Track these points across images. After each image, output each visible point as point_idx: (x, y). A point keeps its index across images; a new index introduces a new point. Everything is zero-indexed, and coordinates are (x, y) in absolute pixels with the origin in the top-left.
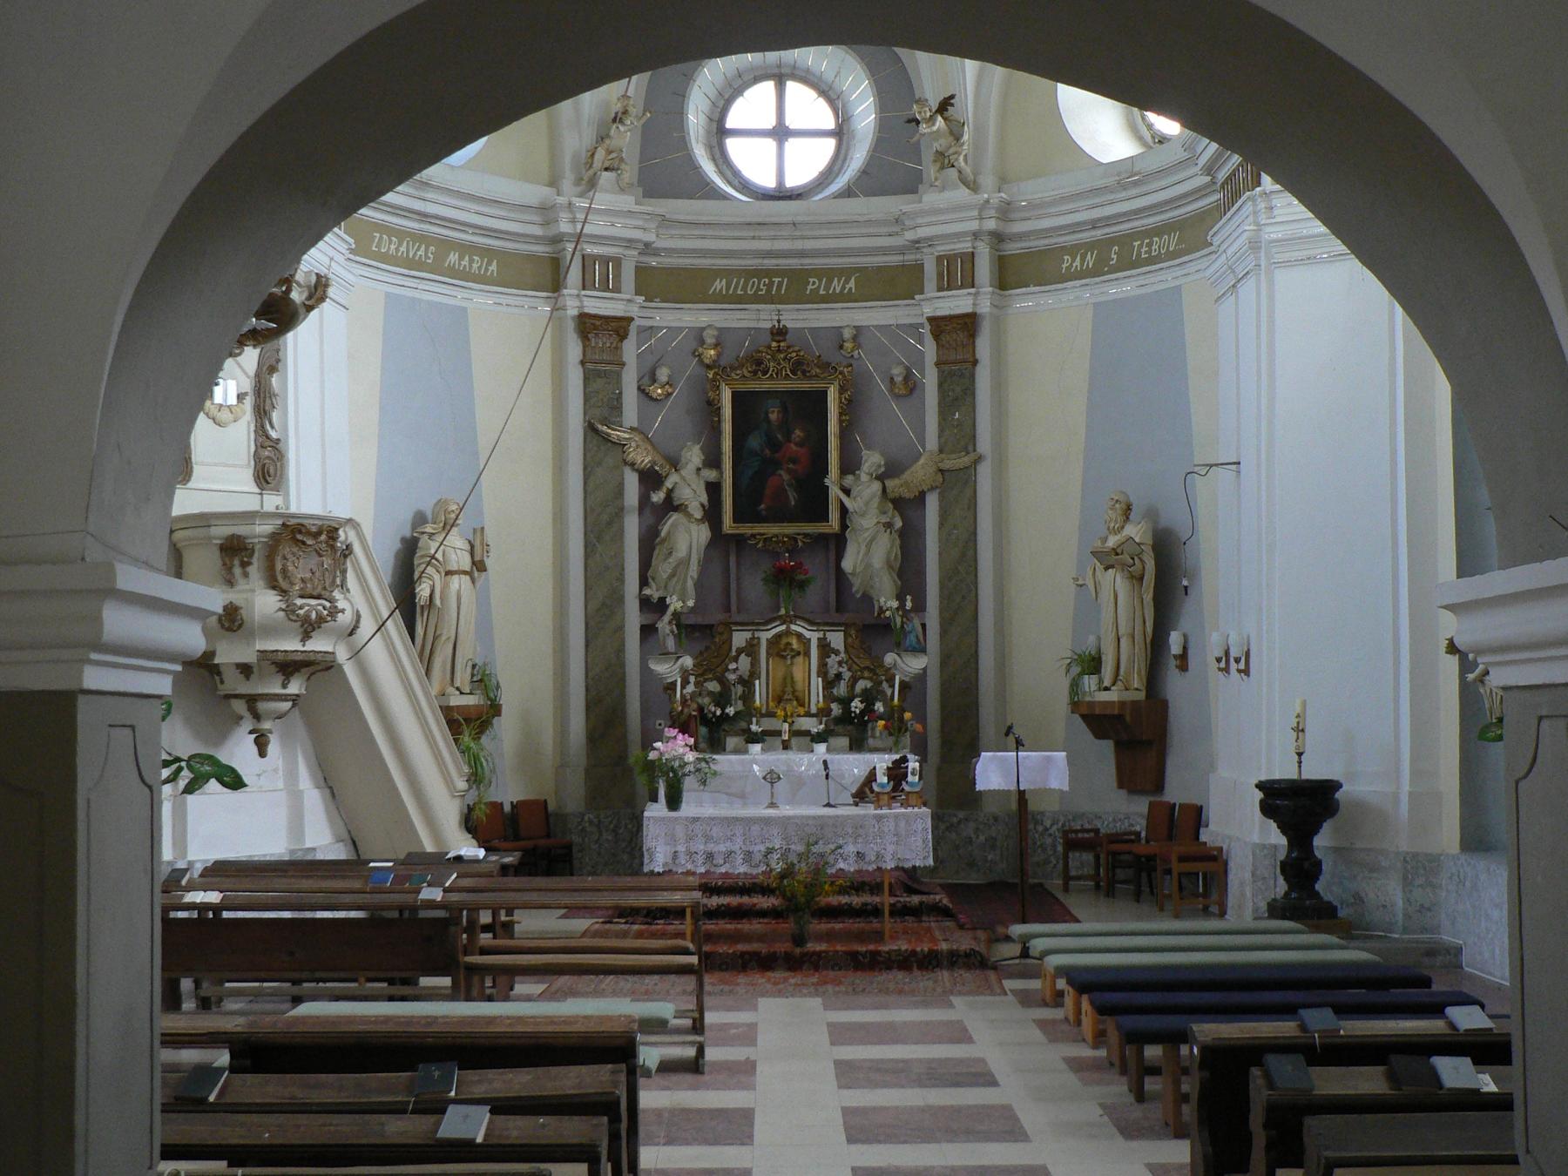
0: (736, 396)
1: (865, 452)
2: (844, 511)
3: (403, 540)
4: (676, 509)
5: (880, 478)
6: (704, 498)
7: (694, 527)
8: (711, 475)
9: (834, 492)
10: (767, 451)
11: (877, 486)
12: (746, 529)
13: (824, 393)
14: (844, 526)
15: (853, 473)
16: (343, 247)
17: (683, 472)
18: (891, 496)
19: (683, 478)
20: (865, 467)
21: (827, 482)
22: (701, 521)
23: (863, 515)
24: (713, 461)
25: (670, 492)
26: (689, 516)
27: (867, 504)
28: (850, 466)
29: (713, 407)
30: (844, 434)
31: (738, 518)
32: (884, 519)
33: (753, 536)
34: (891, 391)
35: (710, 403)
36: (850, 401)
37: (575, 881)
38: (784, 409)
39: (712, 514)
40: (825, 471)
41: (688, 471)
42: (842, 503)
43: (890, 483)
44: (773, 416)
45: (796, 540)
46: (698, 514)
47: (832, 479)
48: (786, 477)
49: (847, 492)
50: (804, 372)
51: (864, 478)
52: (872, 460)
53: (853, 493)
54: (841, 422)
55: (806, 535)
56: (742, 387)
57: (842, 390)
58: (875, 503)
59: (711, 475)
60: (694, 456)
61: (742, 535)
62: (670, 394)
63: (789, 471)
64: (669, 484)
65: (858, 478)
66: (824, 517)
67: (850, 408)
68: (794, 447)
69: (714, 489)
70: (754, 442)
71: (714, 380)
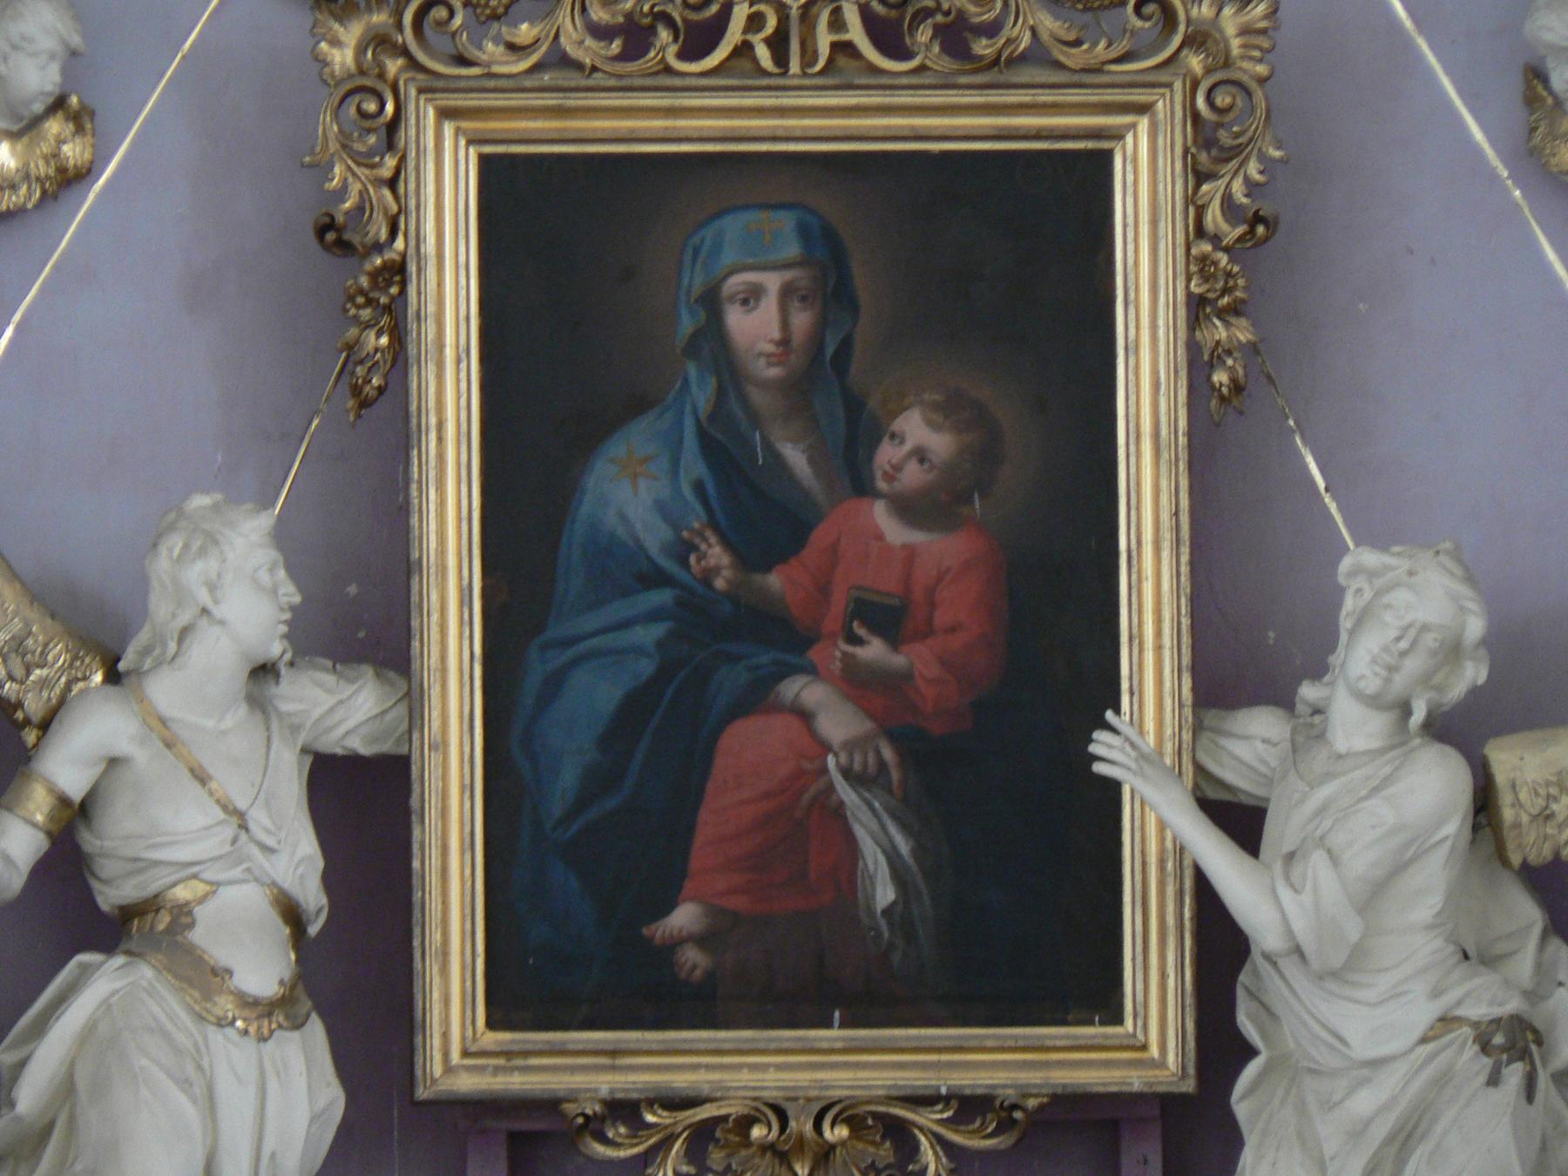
0: (518, 198)
1: (1358, 559)
2: (1219, 944)
3: (210, 778)
4: (113, 931)
5: (1461, 729)
6: (298, 859)
7: (233, 1056)
8: (348, 710)
9: (1159, 822)
10: (716, 554)
11: (1434, 784)
12: (578, 1067)
13: (1085, 179)
14: (1220, 1046)
15: (1285, 701)
16: (1008, 1097)
17: (163, 690)
18: (1531, 845)
19: (165, 734)
20: (1362, 658)
21: (1110, 752)
22: (276, 1012)
23: (1345, 971)
24: (359, 620)
25: (72, 822)
26: (201, 977)
27: (1373, 896)
28: (1247, 662)
29: (359, 263)
30: (1225, 418)
31: (521, 990)
32: (1486, 999)
33: (624, 1110)
34: (1530, 156)
35: (334, 236)
36: (1258, 223)
37: (415, 756)
38: (828, 281)
39: (353, 970)
40: (1099, 691)
41: (194, 683)
42: (1206, 898)
43: (1520, 763)
44: (756, 327)
45: (900, 1134)
46: (262, 968)
47: (1142, 740)
48: (839, 722)
49: (1241, 822)
50: (956, 36)
51: (1353, 726)
52: (1401, 613)
53: (1278, 832)
54: (1199, 363)
55: (970, 1107)
56: (540, 131)
57: (1208, 148)
58: (1429, 888)
59: (348, 710)
60: (232, 584)
61: (550, 1105)
62: (70, 180)
63: (859, 684)
64: (65, 767)
65: (1311, 729)
66: (1099, 995)
67: (1242, 266)
68: (896, 532)
69: (360, 801)
70: (633, 491)
71: (362, 85)
